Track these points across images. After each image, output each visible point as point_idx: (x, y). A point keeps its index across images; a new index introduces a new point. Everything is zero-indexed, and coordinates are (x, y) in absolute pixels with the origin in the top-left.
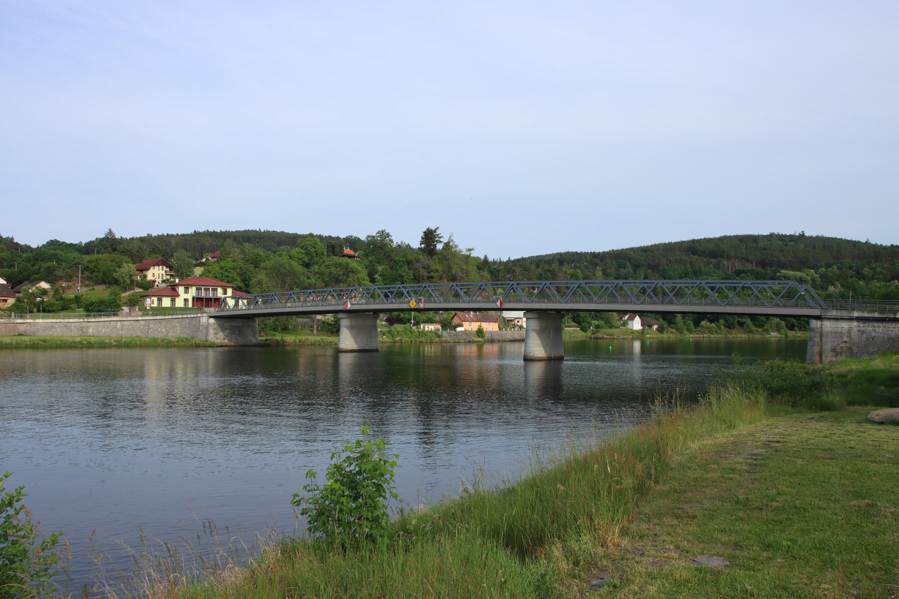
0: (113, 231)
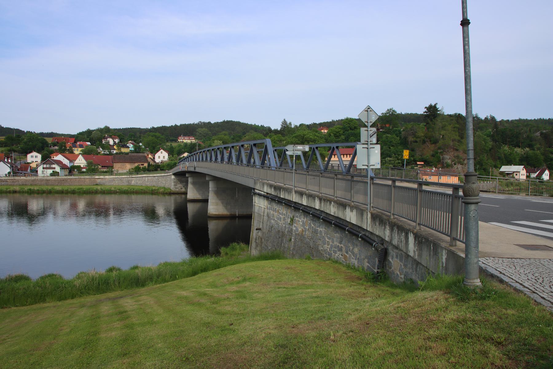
0: (286, 120)
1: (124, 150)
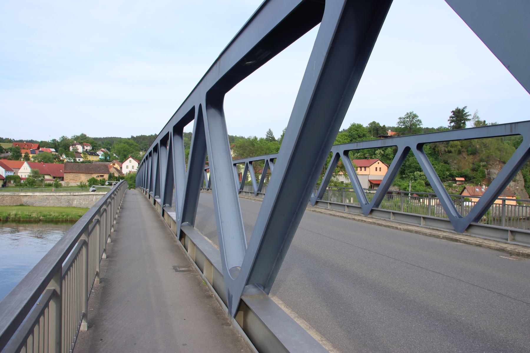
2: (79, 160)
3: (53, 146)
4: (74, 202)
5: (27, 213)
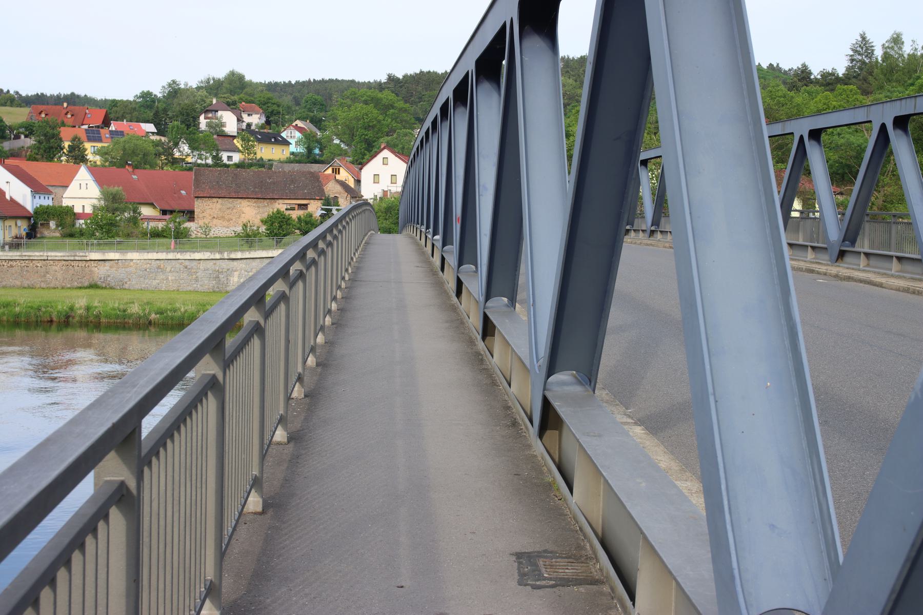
0: (869, 36)
1: (266, 152)
2: (230, 158)
3: (150, 114)
4: (232, 279)
5: (117, 305)
